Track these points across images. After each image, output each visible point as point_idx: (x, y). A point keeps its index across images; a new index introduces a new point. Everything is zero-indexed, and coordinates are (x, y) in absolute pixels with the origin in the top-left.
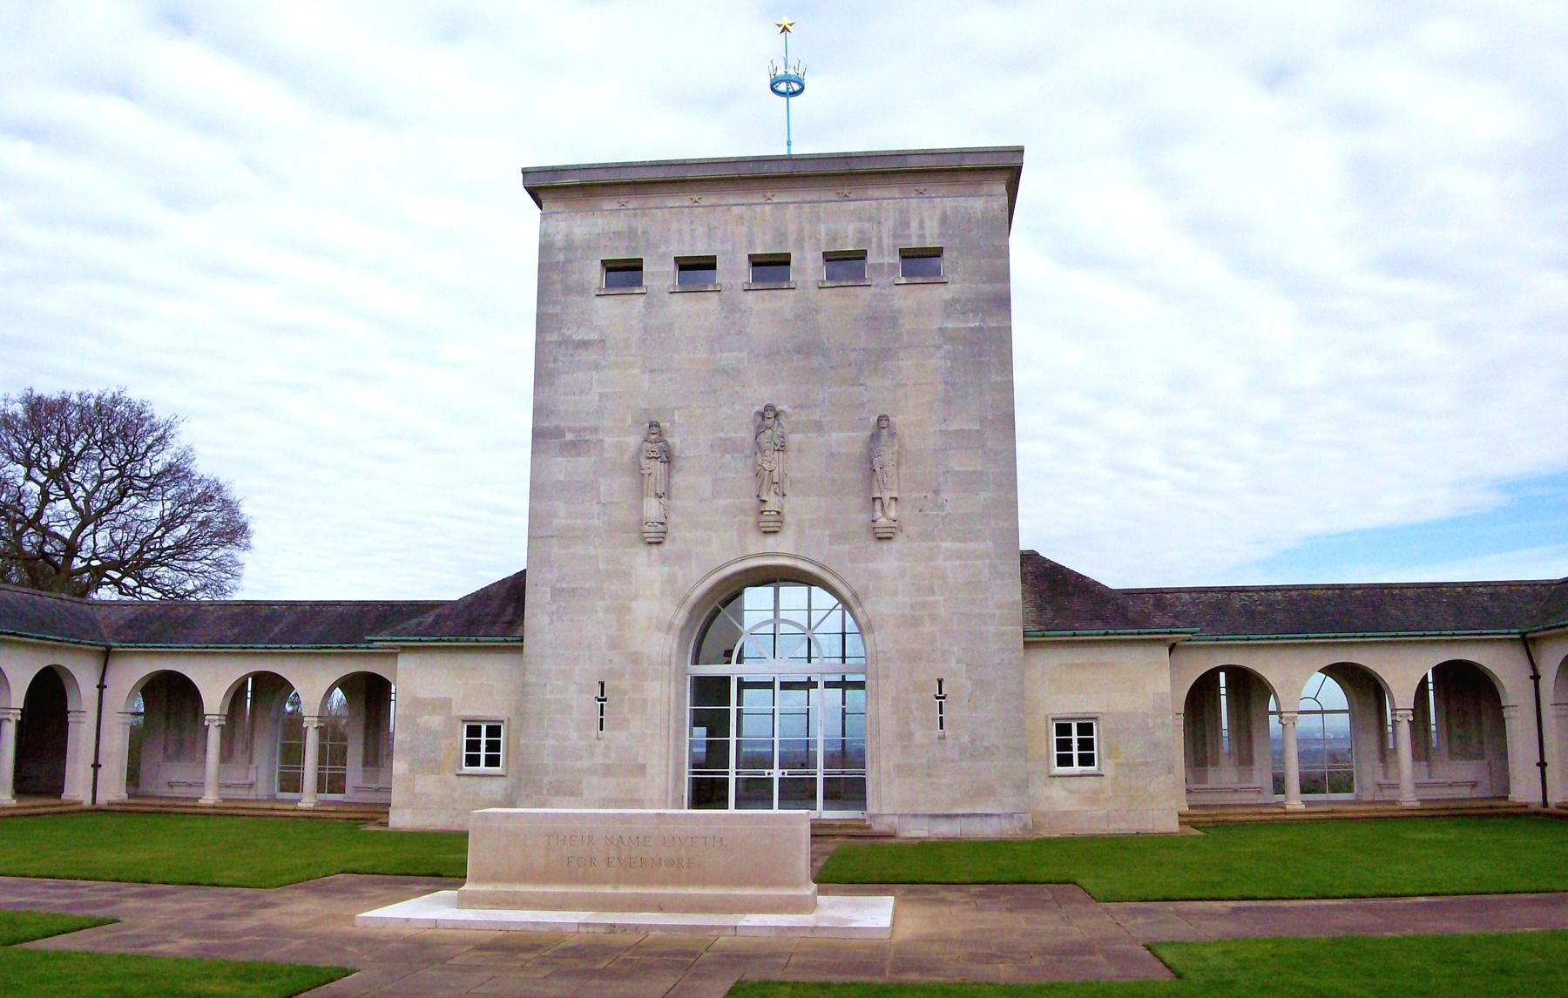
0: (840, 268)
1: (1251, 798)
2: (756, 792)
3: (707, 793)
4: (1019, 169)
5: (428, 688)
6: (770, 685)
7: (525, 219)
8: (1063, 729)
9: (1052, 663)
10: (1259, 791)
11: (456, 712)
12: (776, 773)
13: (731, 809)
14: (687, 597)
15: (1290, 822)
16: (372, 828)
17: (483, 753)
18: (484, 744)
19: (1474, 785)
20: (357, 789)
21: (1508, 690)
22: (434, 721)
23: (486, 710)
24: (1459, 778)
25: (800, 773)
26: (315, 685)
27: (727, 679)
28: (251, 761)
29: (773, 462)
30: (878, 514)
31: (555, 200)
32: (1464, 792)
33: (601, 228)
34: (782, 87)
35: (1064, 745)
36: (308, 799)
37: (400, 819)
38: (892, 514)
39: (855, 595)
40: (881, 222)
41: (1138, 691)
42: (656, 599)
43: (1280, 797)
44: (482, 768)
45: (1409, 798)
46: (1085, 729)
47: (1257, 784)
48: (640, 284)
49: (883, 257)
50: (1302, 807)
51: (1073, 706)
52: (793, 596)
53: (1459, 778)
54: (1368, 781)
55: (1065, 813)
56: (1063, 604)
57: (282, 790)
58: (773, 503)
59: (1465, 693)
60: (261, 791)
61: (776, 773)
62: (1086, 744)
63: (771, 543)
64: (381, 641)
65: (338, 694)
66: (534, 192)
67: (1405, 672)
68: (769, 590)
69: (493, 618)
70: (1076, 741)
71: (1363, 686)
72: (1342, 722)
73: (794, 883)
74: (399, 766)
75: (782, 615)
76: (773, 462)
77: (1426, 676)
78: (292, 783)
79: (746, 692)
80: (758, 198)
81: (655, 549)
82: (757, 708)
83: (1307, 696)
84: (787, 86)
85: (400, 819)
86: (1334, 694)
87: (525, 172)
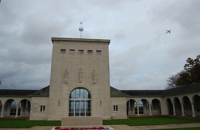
0: (89, 52)
1: (133, 115)
2: (77, 114)
3: (70, 114)
4: (110, 42)
5: (35, 101)
6: (79, 101)
7: (51, 45)
8: (114, 107)
9: (113, 99)
10: (134, 114)
11: (39, 104)
12: (80, 112)
13: (74, 116)
14: (91, 92)
15: (138, 118)
16: (27, 120)
17: (116, 109)
18: (43, 108)
19: (156, 113)
20: (22, 115)
21: (160, 101)
22: (36, 106)
23: (43, 104)
24: (156, 112)
25: (83, 112)
26: (17, 101)
27: (26, 100)
28: (7, 111)
29: (81, 74)
30: (94, 81)
31: (56, 42)
32: (155, 114)
33: (62, 45)
34: (80, 30)
35: (114, 108)
36: (16, 116)
37: (31, 119)
38: (96, 81)
39: (91, 91)
40: (94, 47)
41: (122, 102)
42: (66, 90)
43: (136, 115)
44: (116, 111)
45: (151, 114)
46: (117, 106)
47: (133, 113)
48: (65, 52)
49: (94, 51)
50: (185, 116)
51: (115, 104)
52: (82, 90)
53: (156, 112)
54: (145, 113)
55: (115, 117)
56: (115, 93)
57: (11, 115)
58: (81, 79)
59: (156, 103)
60: (8, 116)
61: (80, 112)
62: (117, 108)
63: (80, 84)
64: (30, 95)
65: (20, 103)
66: (53, 41)
67: (150, 100)
68: (79, 89)
69: (45, 92)
70: (116, 108)
71: (144, 101)
72: (142, 106)
73: (101, 125)
74: (31, 112)
75: (81, 93)
76: (81, 74)
77: (128, 101)
78: (136, 113)
79: (76, 102)
80: (80, 43)
81: (66, 85)
82: (78, 104)
83: (139, 102)
84: (81, 30)
85: (31, 119)
86: (141, 103)
87: (52, 38)
